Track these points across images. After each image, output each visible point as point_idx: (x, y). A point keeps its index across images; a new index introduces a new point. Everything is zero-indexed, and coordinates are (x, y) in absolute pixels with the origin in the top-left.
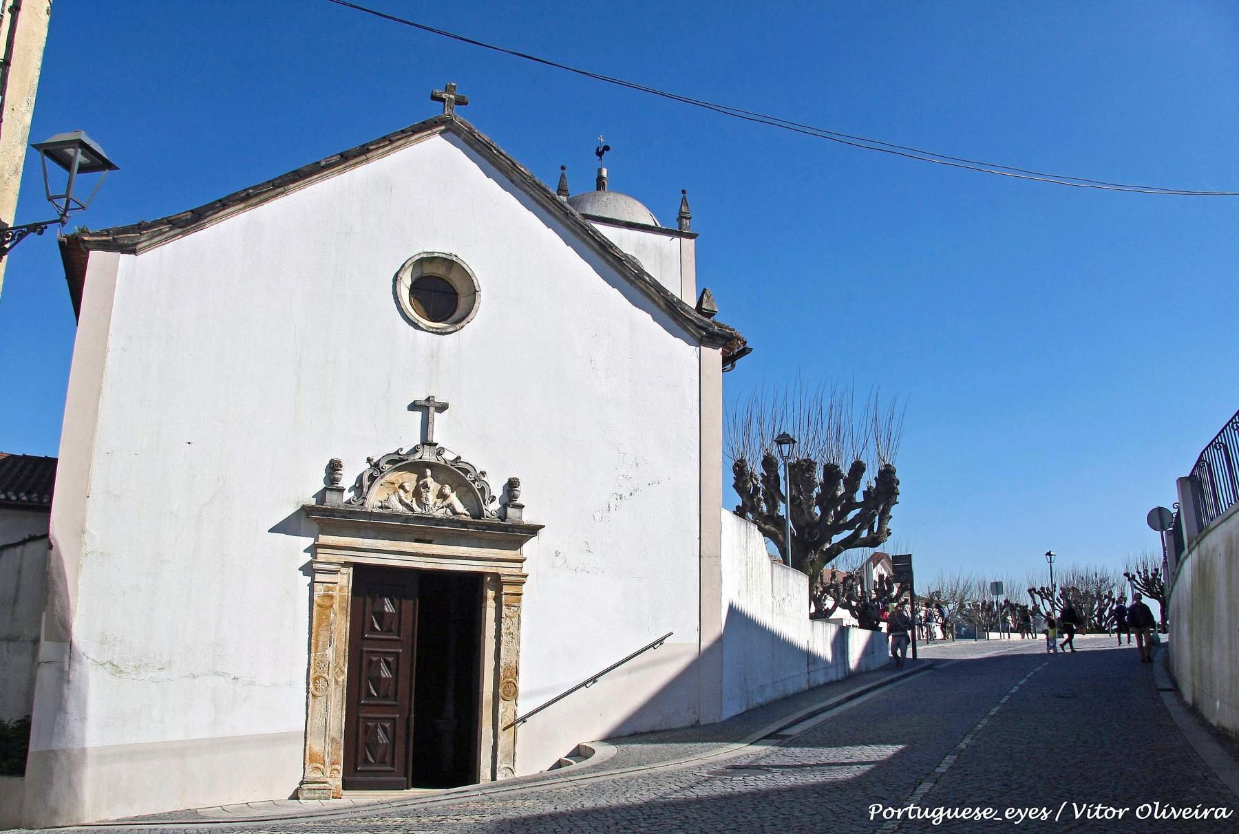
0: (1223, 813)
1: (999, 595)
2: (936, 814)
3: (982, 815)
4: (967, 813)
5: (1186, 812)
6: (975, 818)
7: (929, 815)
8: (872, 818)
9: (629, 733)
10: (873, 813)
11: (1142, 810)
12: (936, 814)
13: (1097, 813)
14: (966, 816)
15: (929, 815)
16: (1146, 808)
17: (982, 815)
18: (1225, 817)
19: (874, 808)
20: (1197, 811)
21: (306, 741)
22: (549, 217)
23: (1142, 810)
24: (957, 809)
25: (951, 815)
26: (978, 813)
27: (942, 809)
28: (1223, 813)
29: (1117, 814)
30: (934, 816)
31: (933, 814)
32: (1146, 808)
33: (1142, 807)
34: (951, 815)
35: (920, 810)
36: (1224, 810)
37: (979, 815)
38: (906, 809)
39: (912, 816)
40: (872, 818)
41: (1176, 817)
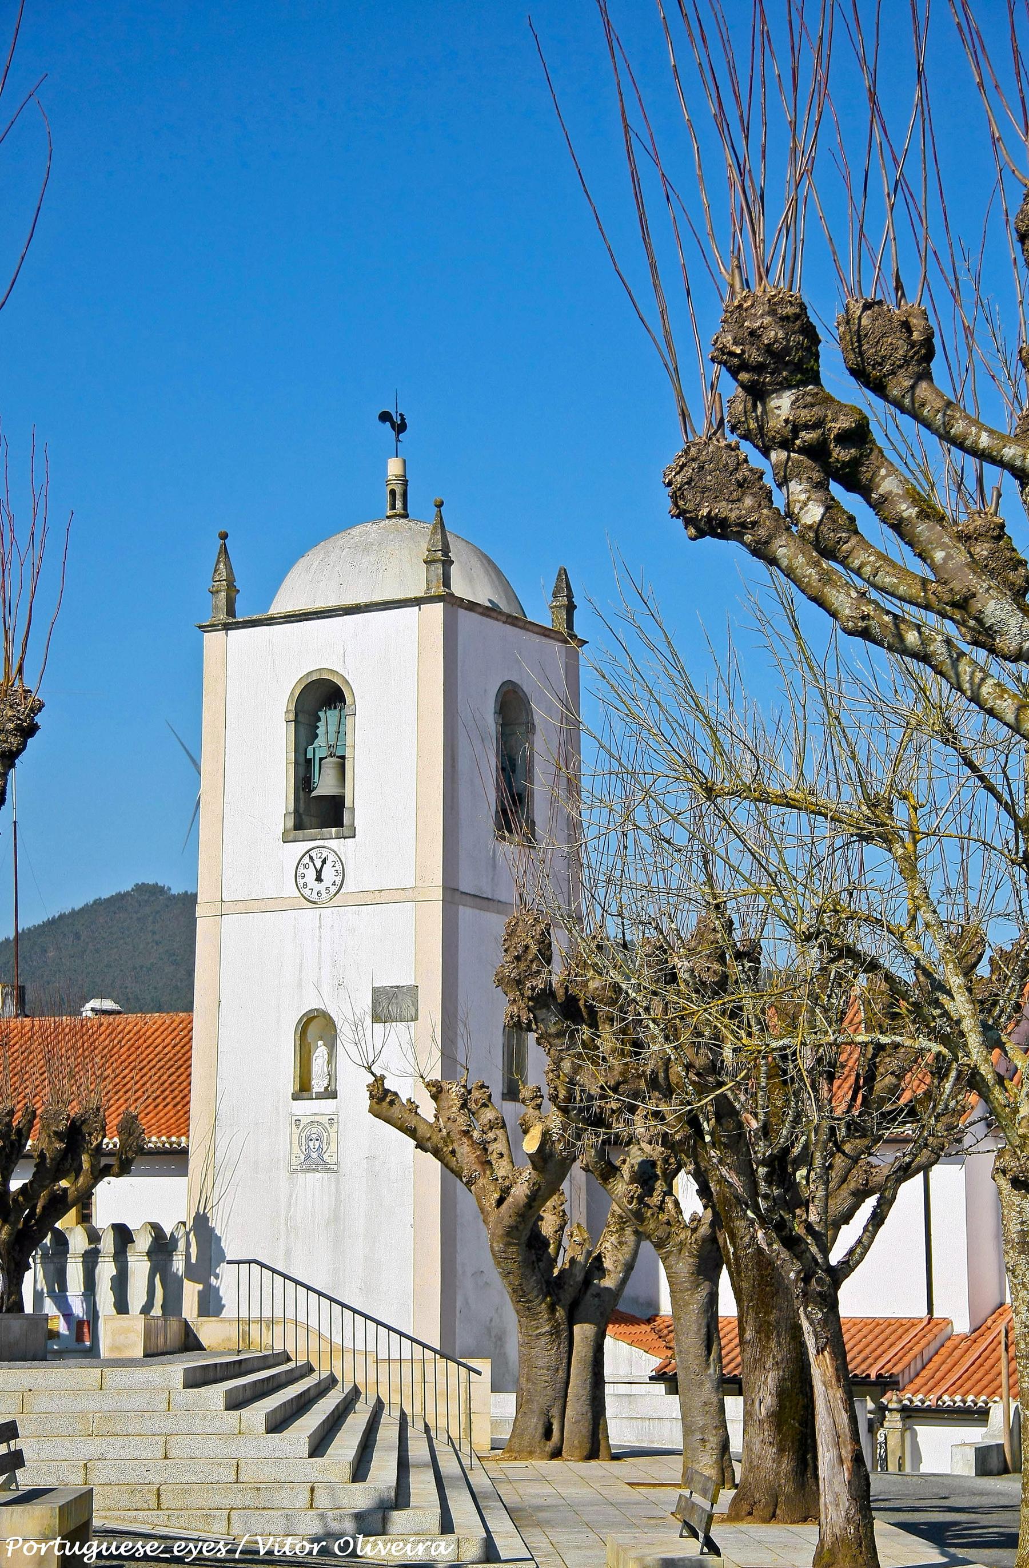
0: (442, 1549)
1: (97, 1523)
2: (88, 1550)
3: (145, 1551)
4: (399, 1548)
5: (179, 1547)
6: (137, 1555)
7: (116, 1550)
8: (9, 1555)
9: (703, 1347)
10: (10, 1548)
11: (342, 1545)
12: (88, 1550)
13: (113, 1548)
14: (126, 1551)
15: (116, 1550)
16: (347, 1543)
17: (145, 1551)
18: (444, 1553)
19: (12, 1543)
20: (409, 1546)
21: (942, 197)
22: (356, 1463)
23: (342, 1545)
24: (78, 1543)
25: (107, 1551)
26: (140, 1548)
27: (95, 1543)
28: (442, 1549)
29: (39, 1549)
30: (86, 1552)
31: (84, 1550)
32: (347, 1543)
33: (342, 1541)
34: (107, 1551)
35: (68, 1544)
36: (443, 1544)
37: (142, 1551)
38: (52, 1543)
39: (59, 1551)
40: (9, 1555)
41: (383, 1553)
